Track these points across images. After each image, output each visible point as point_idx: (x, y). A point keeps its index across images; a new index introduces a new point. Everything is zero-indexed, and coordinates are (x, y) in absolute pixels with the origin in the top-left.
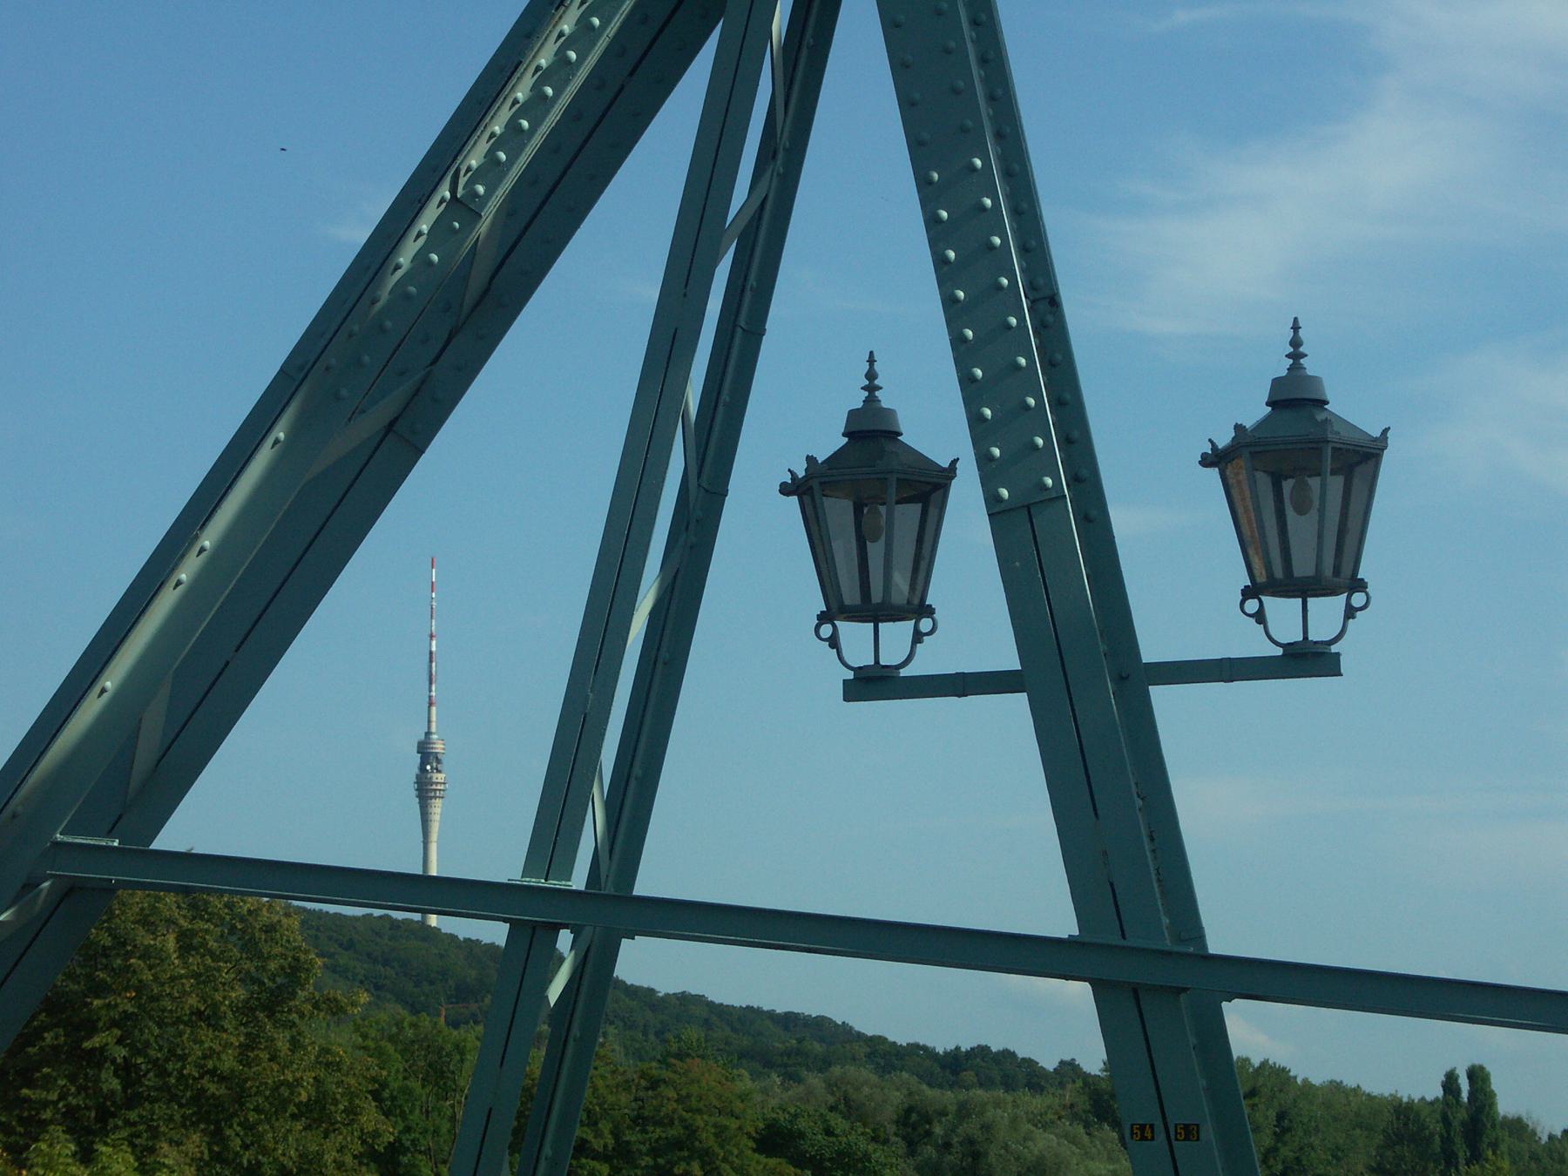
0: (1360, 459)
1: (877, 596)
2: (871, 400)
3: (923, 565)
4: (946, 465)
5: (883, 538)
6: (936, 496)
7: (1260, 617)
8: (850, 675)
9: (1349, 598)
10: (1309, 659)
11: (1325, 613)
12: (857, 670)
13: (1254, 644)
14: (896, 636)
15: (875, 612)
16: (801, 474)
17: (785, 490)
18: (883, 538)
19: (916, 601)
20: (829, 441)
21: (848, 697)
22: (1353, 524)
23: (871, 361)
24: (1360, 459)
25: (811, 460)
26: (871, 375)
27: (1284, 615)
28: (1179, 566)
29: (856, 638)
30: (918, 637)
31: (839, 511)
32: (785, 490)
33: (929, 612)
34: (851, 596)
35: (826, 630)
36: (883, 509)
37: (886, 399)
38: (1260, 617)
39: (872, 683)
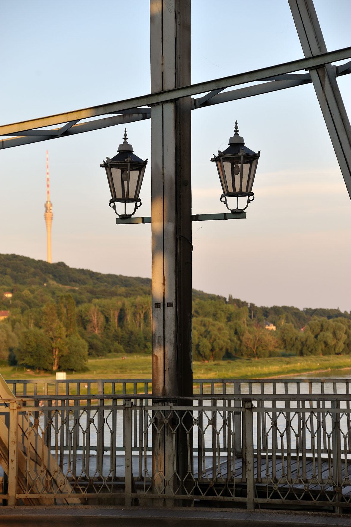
0: (252, 158)
1: (238, 190)
2: (125, 142)
3: (251, 181)
4: (257, 153)
5: (239, 174)
6: (254, 162)
7: (225, 202)
8: (118, 217)
9: (136, 204)
10: (238, 214)
11: (243, 200)
12: (232, 210)
13: (223, 210)
14: (131, 206)
15: (125, 200)
16: (217, 155)
17: (102, 166)
18: (239, 174)
19: (249, 191)
20: (113, 153)
21: (117, 224)
22: (140, 184)
23: (236, 123)
24: (252, 158)
25: (107, 158)
26: (125, 135)
27: (232, 201)
28: (206, 189)
29: (120, 206)
30: (136, 207)
31: (227, 166)
32: (102, 166)
33: (252, 194)
34: (231, 190)
35: (223, 199)
36: (239, 165)
37: (129, 142)
38: (225, 202)
39: (125, 219)
